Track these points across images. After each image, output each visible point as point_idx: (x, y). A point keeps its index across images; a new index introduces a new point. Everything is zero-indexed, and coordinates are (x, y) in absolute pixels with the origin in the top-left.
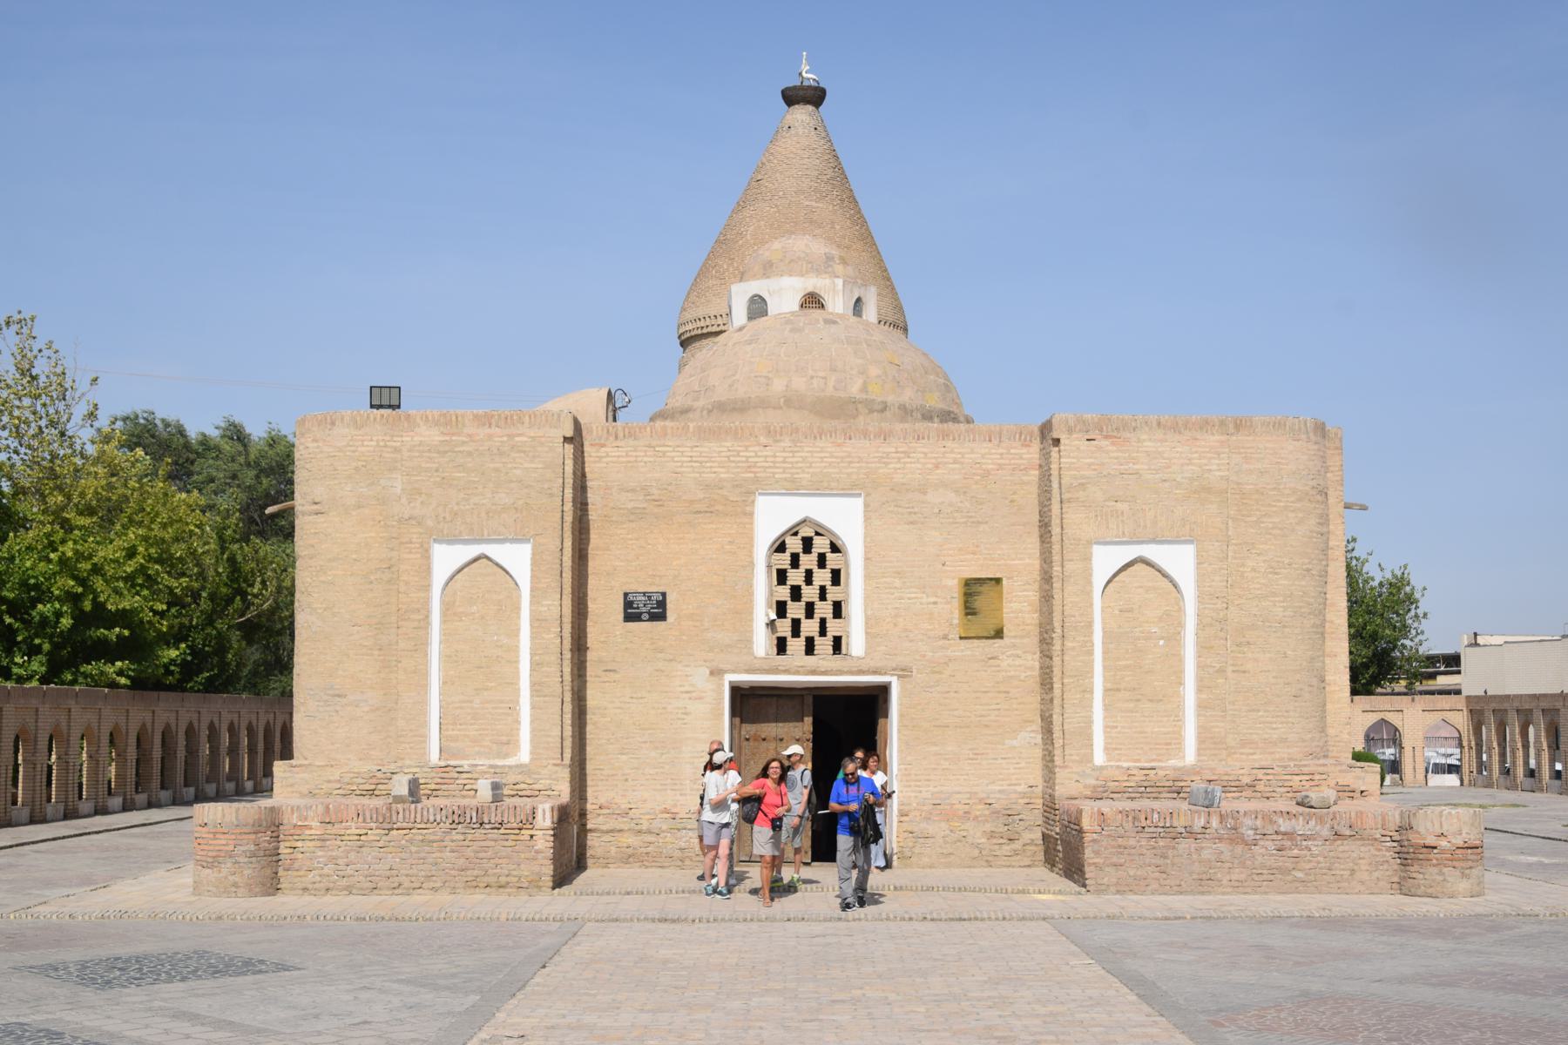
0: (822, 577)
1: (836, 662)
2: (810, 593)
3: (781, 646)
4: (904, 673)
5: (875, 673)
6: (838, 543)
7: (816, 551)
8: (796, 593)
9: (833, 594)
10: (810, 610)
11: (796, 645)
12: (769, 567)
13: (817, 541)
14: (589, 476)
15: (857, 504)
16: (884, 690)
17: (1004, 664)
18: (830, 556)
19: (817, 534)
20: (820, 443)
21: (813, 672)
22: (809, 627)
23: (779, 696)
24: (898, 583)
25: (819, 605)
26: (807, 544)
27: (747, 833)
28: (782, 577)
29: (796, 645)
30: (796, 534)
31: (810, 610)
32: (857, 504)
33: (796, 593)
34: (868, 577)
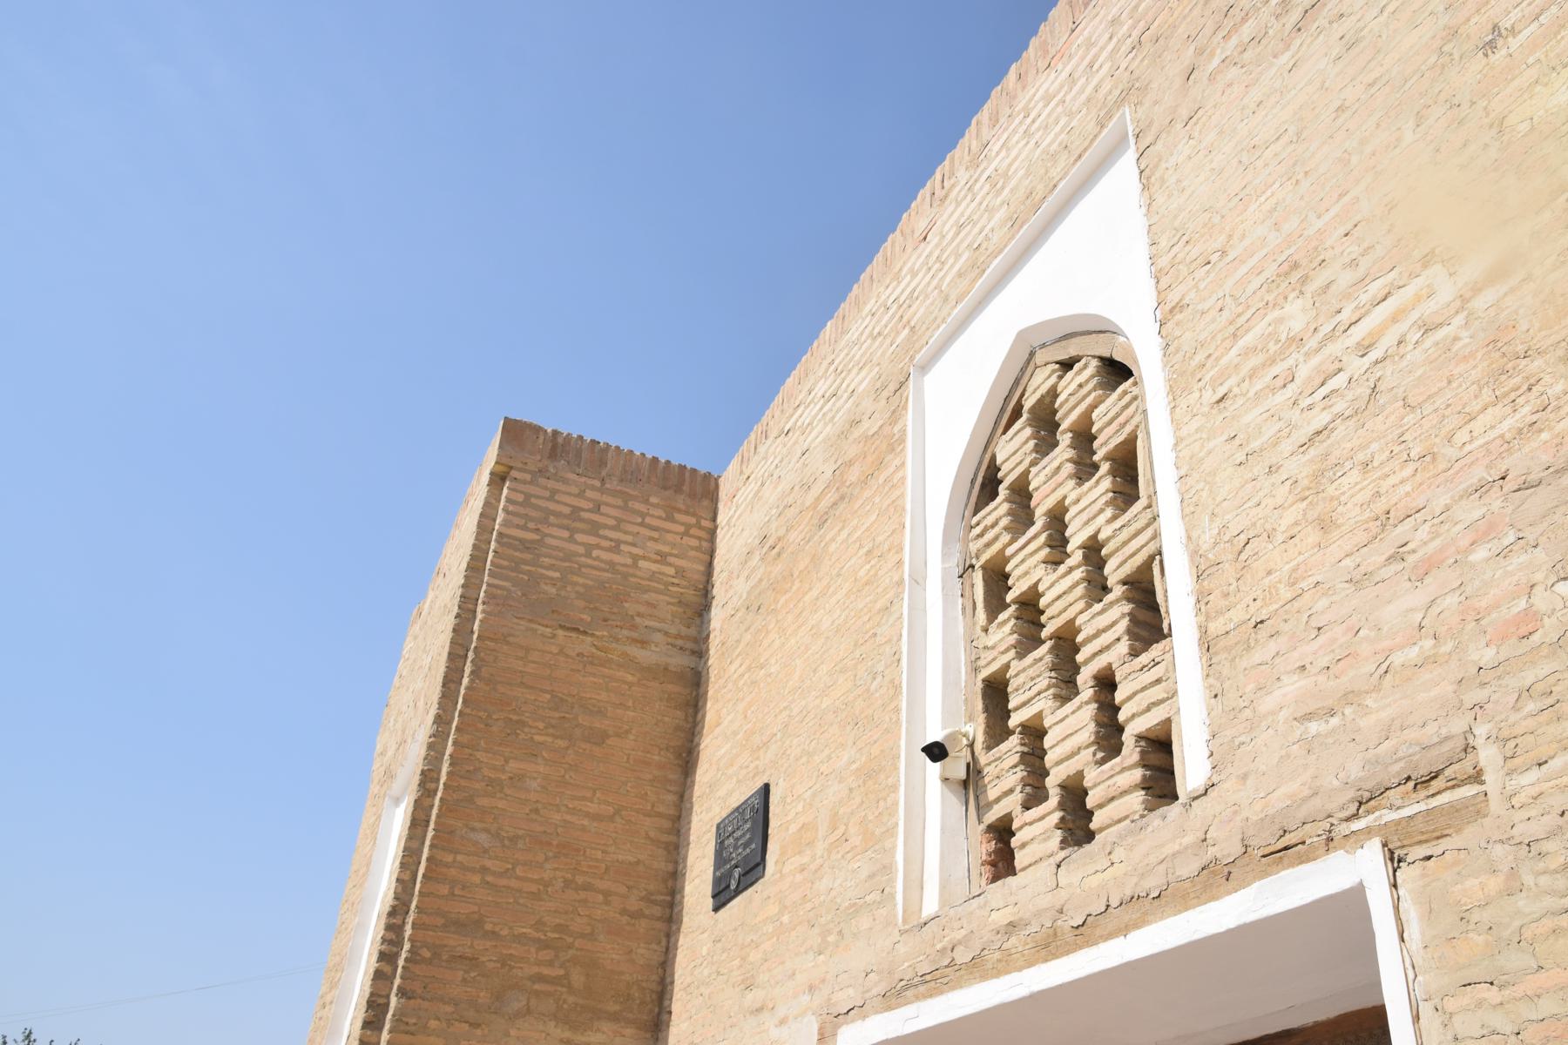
11: (1038, 831)
24: (1296, 314)
29: (1038, 831)
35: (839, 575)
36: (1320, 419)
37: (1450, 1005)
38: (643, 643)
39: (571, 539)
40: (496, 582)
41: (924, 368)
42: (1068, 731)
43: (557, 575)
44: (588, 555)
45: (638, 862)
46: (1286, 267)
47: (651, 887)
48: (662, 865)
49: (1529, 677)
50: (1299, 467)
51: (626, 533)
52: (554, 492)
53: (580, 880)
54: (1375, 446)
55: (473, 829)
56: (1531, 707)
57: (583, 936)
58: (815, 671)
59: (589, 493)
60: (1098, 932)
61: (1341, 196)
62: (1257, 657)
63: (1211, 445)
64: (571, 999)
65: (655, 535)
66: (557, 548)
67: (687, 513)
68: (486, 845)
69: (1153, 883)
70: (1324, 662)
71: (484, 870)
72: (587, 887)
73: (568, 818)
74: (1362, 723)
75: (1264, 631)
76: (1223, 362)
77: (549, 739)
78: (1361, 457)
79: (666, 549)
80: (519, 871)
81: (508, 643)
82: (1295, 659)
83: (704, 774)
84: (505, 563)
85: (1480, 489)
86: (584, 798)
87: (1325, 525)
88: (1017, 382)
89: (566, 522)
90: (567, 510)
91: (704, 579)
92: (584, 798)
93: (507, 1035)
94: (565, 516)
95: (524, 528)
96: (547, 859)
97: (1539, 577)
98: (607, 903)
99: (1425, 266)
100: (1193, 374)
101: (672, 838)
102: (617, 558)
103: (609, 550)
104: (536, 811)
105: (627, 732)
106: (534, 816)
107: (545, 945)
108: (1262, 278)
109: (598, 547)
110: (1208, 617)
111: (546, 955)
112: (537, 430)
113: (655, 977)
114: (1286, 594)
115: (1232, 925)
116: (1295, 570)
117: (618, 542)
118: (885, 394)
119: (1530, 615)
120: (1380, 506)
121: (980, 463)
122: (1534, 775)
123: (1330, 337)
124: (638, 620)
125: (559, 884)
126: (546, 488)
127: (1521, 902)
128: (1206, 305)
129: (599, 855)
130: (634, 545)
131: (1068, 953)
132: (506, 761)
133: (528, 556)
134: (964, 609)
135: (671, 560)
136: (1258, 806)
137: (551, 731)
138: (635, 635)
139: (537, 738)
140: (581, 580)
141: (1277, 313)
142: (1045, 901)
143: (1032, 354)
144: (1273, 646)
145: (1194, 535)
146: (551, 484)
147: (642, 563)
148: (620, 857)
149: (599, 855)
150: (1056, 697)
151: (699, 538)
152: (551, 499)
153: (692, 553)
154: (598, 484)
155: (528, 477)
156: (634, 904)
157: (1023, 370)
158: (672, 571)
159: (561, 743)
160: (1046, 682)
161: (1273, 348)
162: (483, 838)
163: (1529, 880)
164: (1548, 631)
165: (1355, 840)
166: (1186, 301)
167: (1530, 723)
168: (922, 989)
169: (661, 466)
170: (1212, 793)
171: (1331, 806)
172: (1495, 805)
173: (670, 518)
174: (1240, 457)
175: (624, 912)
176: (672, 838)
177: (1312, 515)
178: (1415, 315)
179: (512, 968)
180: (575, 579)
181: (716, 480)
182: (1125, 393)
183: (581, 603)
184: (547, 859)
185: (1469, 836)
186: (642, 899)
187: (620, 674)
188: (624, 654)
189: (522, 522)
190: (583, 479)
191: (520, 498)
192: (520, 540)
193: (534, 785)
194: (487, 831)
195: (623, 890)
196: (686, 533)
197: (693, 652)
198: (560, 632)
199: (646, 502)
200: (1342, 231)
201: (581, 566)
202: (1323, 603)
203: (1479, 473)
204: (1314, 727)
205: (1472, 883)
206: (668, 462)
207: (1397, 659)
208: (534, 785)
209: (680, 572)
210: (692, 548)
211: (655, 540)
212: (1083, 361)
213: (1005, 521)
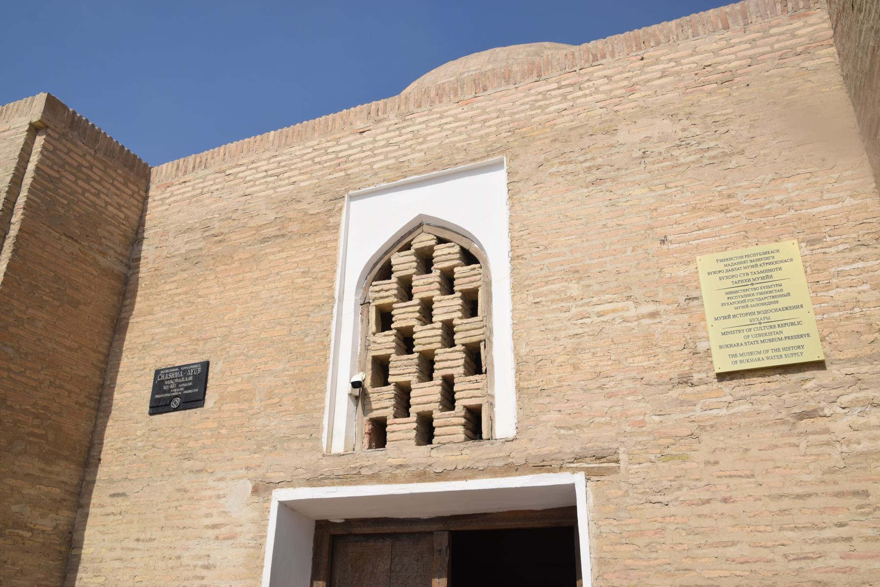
1: (475, 452)
3: (378, 434)
4: (600, 463)
5: (541, 468)
6: (473, 249)
11: (401, 431)
13: (440, 251)
14: (148, 224)
15: (496, 181)
16: (566, 516)
17: (840, 427)
19: (441, 241)
20: (438, 108)
21: (422, 476)
22: (425, 396)
23: (395, 536)
24: (575, 289)
26: (426, 261)
28: (385, 319)
29: (401, 431)
30: (408, 247)
32: (496, 181)
33: (406, 341)
34: (517, 287)
35: (277, 274)
36: (580, 331)
37: (600, 523)
38: (104, 254)
39: (75, 183)
40: (33, 197)
41: (352, 198)
42: (425, 396)
43: (65, 202)
44: (83, 195)
45: (86, 376)
46: (573, 269)
47: (91, 391)
48: (97, 380)
49: (640, 439)
50: (570, 344)
51: (104, 187)
52: (70, 150)
53: (58, 382)
54: (598, 349)
55: (5, 345)
56: (639, 447)
57: (56, 413)
58: (254, 316)
59: (88, 157)
60: (449, 476)
61: (600, 257)
62: (541, 401)
63: (530, 318)
64: (47, 447)
65: (118, 192)
66: (67, 185)
67: (134, 184)
68: (12, 356)
69: (481, 465)
70: (569, 412)
71: (9, 370)
72: (61, 387)
73: (55, 346)
74: (582, 436)
75: (544, 393)
76: (540, 289)
77: (51, 300)
78: (593, 350)
79: (122, 202)
80: (28, 373)
81: (35, 237)
82: (557, 406)
83: (133, 337)
84: (39, 187)
85: (634, 379)
86: (64, 337)
87: (575, 367)
88: (410, 233)
89: (74, 171)
90: (75, 164)
91: (137, 224)
92: (64, 337)
93: (13, 464)
94: (74, 168)
95: (51, 168)
96: (42, 368)
97: (648, 412)
98: (70, 397)
99: (627, 300)
100: (525, 287)
101: (104, 366)
102: (98, 201)
103: (94, 195)
104: (39, 340)
105: (90, 303)
106: (38, 343)
107: (36, 416)
108: (562, 268)
109: (88, 191)
110: (520, 379)
111: (37, 422)
112: (65, 107)
113: (87, 439)
114: (556, 384)
115: (519, 486)
116: (561, 377)
117: (100, 192)
118: (323, 197)
119: (643, 421)
120: (598, 370)
121: (381, 259)
122: (637, 466)
123: (587, 304)
124: (103, 240)
125: (47, 383)
126: (65, 146)
127: (628, 499)
128: (535, 264)
129: (68, 370)
130: (107, 196)
131: (432, 481)
132: (27, 308)
133: (51, 186)
134: (362, 320)
135: (124, 209)
136: (536, 451)
137: (52, 295)
138: (101, 249)
139: (44, 297)
140: (78, 209)
141: (566, 284)
142: (424, 460)
143: (421, 225)
144: (548, 400)
145: (518, 348)
146: (69, 145)
147: (109, 208)
148: (79, 373)
149: (68, 370)
150: (418, 377)
151: (138, 200)
152: (67, 154)
153: (134, 208)
154: (93, 153)
155: (57, 136)
156: (82, 399)
157: (414, 229)
158: (122, 216)
159: (57, 303)
160: (415, 370)
161: (563, 296)
162: (10, 351)
163: (631, 494)
164: (648, 428)
165: (575, 470)
166: (525, 257)
167: (638, 452)
168: (336, 481)
169: (125, 152)
170: (515, 442)
171: (564, 457)
172: (622, 470)
173: (125, 185)
174: (543, 328)
175: (77, 403)
176: (104, 366)
177: (571, 362)
178: (621, 314)
179: (19, 427)
180: (75, 207)
181: (150, 169)
182: (474, 269)
183: (76, 223)
184: (42, 368)
185: (613, 477)
186: (86, 397)
187: (90, 269)
188: (94, 258)
189: (51, 164)
190: (86, 147)
191: (51, 148)
192: (46, 174)
193: (40, 324)
194: (11, 347)
195: (78, 390)
196: (132, 196)
197: (126, 265)
198: (64, 238)
199: (115, 171)
200: (599, 270)
201: (79, 200)
202: (570, 392)
203: (634, 374)
204: (562, 431)
205: (612, 491)
206: (129, 151)
207: (597, 420)
208: (40, 324)
209: (127, 218)
210: (135, 206)
211: (117, 196)
212: (452, 244)
213: (395, 292)
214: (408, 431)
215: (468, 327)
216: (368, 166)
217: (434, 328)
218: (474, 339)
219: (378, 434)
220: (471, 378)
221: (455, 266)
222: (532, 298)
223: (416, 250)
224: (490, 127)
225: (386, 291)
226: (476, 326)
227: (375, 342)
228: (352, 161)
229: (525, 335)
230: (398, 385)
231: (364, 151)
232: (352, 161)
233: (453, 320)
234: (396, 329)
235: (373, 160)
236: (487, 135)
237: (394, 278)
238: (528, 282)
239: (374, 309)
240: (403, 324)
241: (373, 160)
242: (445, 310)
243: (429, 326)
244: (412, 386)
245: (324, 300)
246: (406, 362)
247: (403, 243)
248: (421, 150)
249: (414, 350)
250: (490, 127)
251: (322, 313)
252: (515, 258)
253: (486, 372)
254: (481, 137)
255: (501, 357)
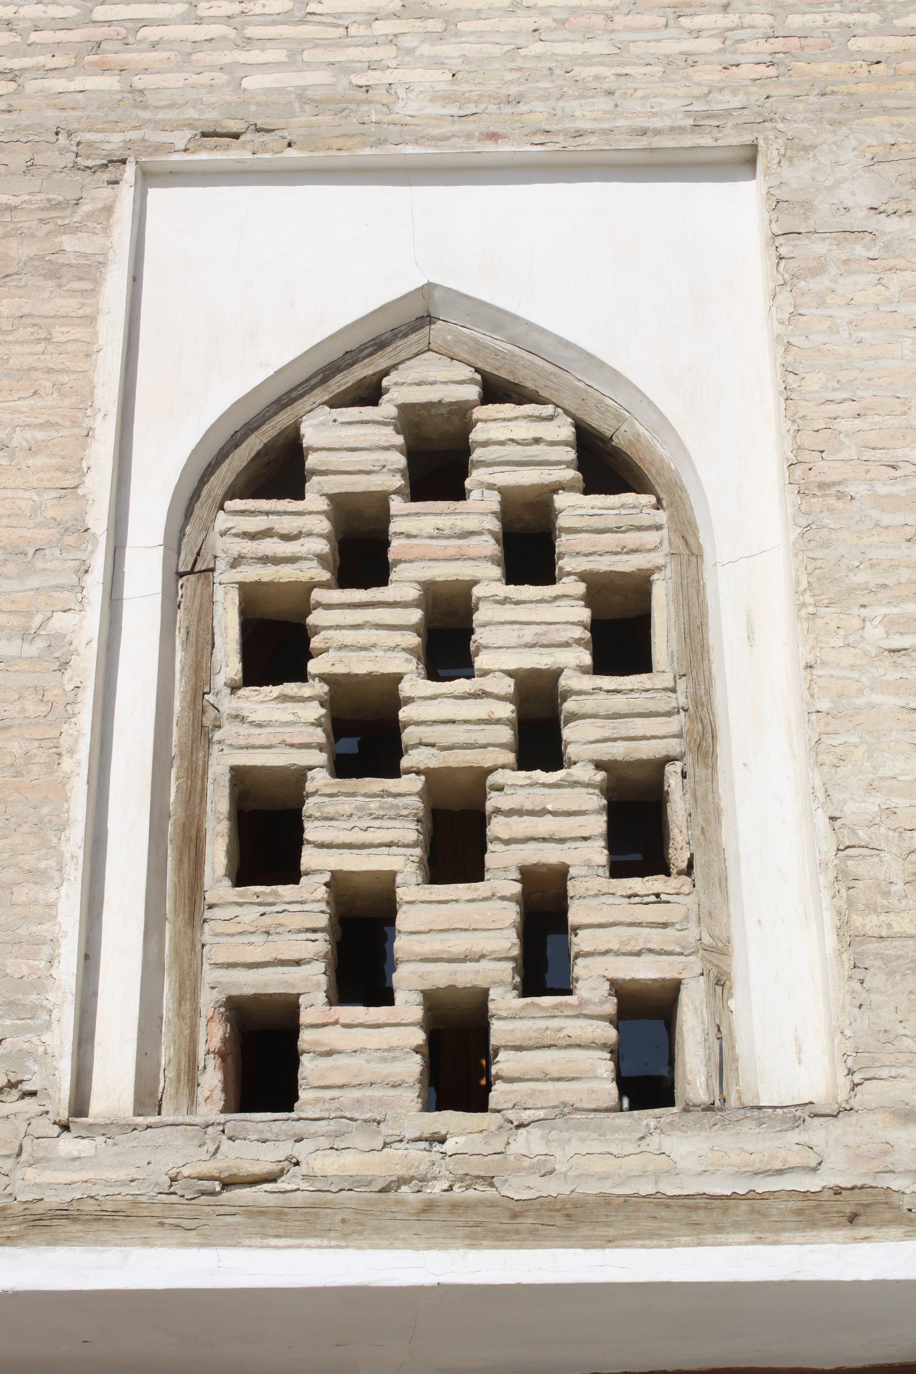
0: (531, 630)
2: (456, 724)
6: (629, 434)
7: (486, 487)
8: (366, 735)
9: (606, 721)
10: (455, 841)
11: (362, 1056)
12: (188, 570)
13: (494, 426)
18: (574, 508)
19: (495, 390)
22: (453, 936)
25: (515, 792)
26: (438, 464)
27: (835, 1221)
28: (275, 645)
29: (362, 1056)
30: (369, 393)
31: (455, 841)
33: (366, 735)
34: (822, 589)
63: (876, 698)
88: (379, 345)
100: (851, 590)
110: (851, 903)
121: (250, 428)
128: (886, 519)
145: (836, 796)
166: (851, 489)
170: (844, 1118)
212: (549, 410)
214: (390, 1053)
215: (619, 703)
216: (222, 78)
217: (483, 695)
218: (646, 751)
219: (263, 1060)
220: (635, 884)
221: (557, 487)
222: (880, 632)
223: (404, 408)
224: (697, 33)
225: (287, 538)
226: (652, 706)
227: (239, 718)
228: (154, 46)
229: (859, 752)
230: (339, 885)
231: (199, 21)
232: (154, 46)
233: (558, 672)
234: (324, 678)
235: (242, 57)
236: (690, 60)
237: (314, 498)
238: (863, 577)
239: (234, 597)
240: (360, 665)
241: (242, 57)
242: (529, 634)
243: (461, 685)
244: (402, 894)
245: (42, 535)
246: (374, 804)
247: (350, 373)
248: (438, 63)
249: (405, 762)
250: (697, 33)
251: (35, 582)
252: (811, 485)
253: (689, 870)
254: (669, 61)
255: (762, 816)
